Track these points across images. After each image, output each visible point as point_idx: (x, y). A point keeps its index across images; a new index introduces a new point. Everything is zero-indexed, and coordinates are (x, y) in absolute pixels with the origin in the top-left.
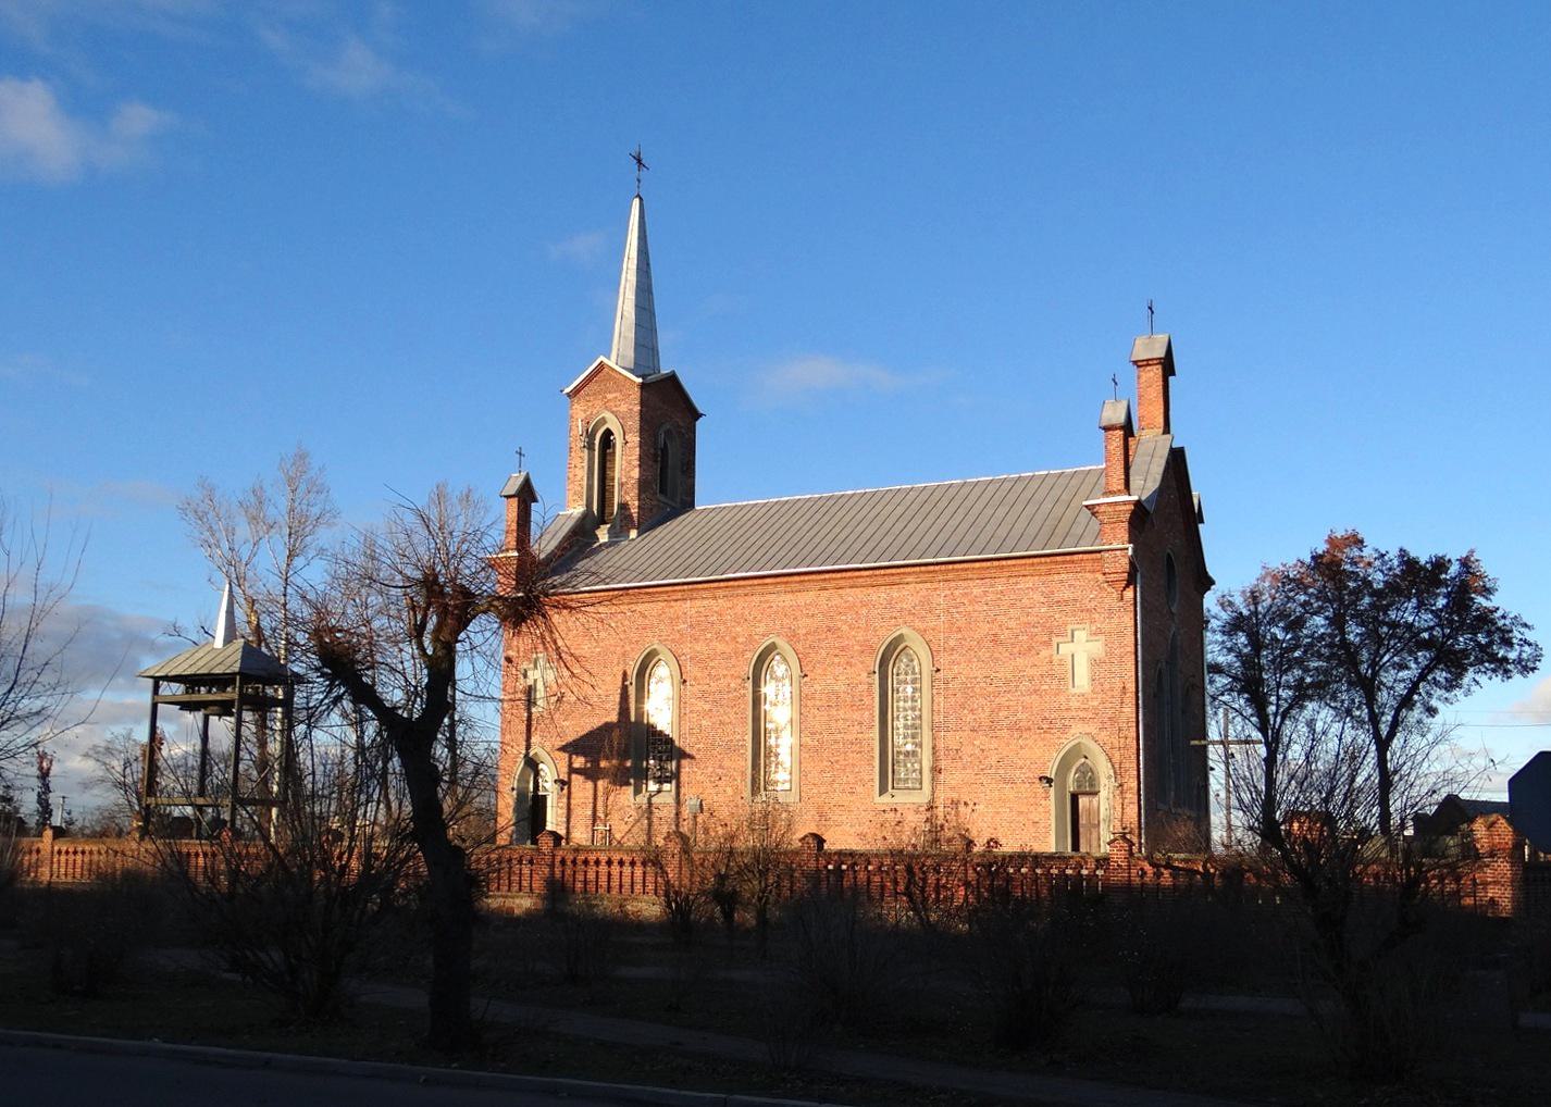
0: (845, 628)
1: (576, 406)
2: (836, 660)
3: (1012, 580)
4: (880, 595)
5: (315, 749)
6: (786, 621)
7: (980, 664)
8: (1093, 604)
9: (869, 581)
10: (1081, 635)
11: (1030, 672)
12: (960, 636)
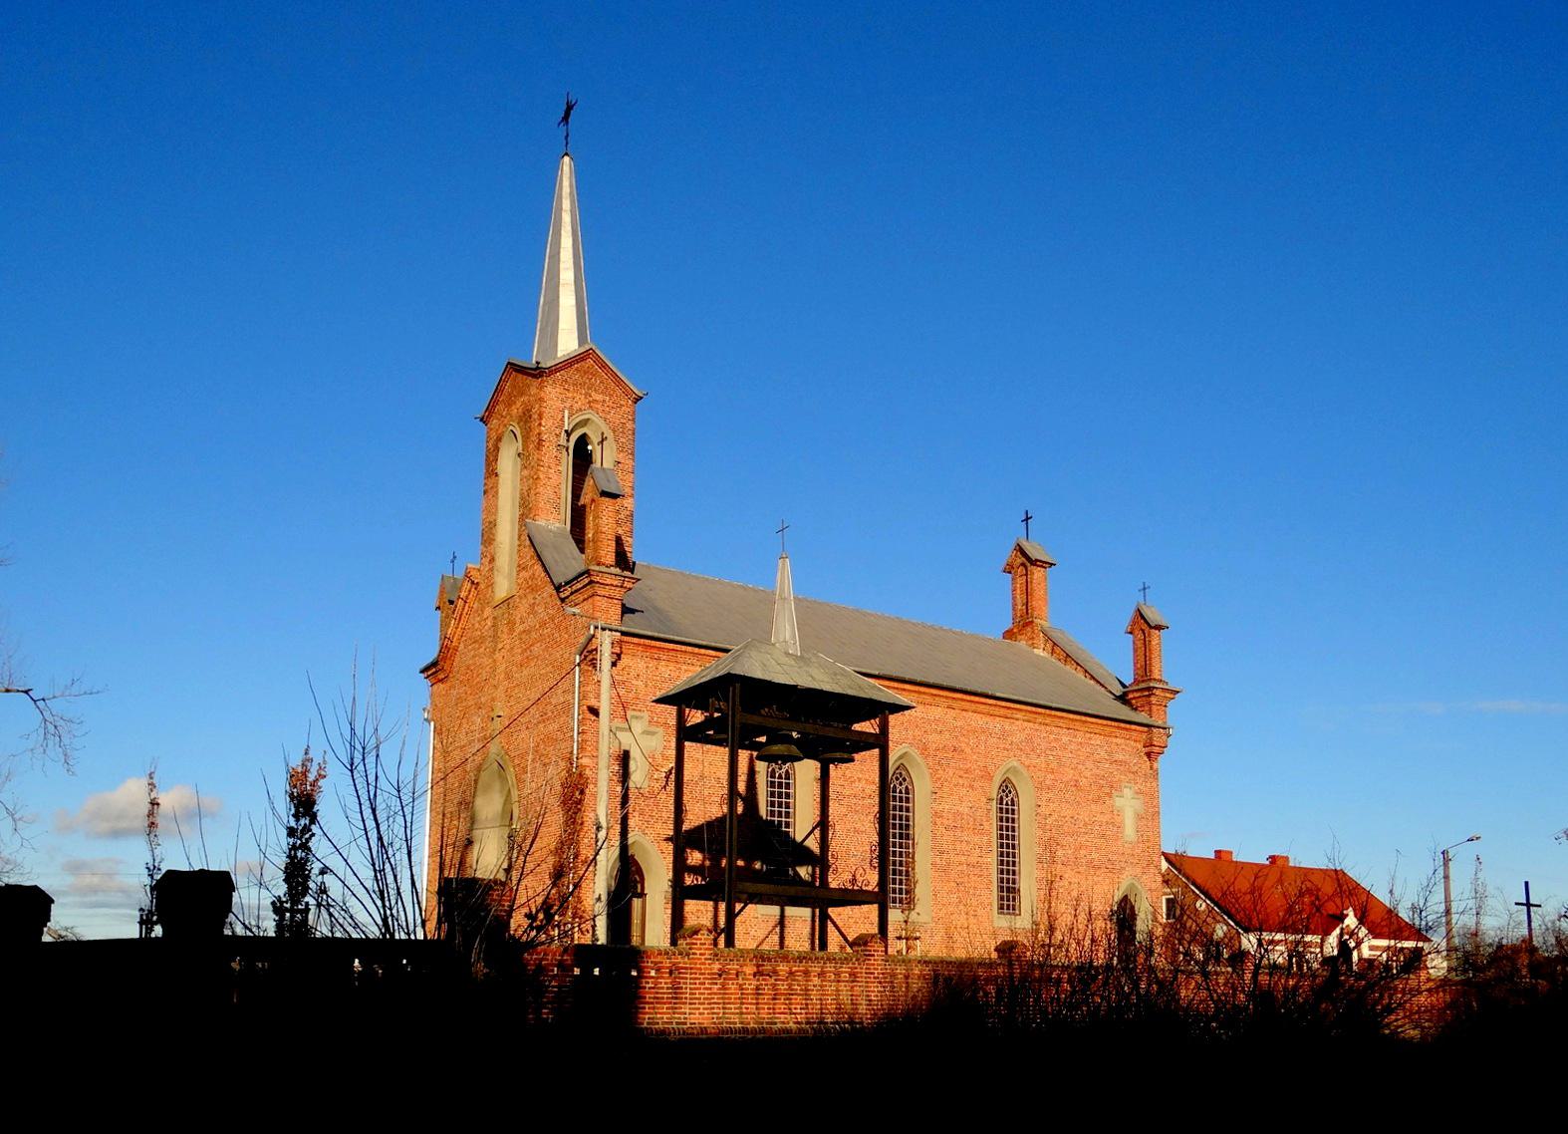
0: (968, 750)
1: (549, 389)
2: (961, 782)
3: (1088, 735)
4: (996, 725)
5: (1455, 918)
6: (917, 733)
7: (1068, 806)
8: (1136, 768)
9: (1003, 712)
10: (1128, 792)
11: (1100, 818)
12: (1053, 777)
